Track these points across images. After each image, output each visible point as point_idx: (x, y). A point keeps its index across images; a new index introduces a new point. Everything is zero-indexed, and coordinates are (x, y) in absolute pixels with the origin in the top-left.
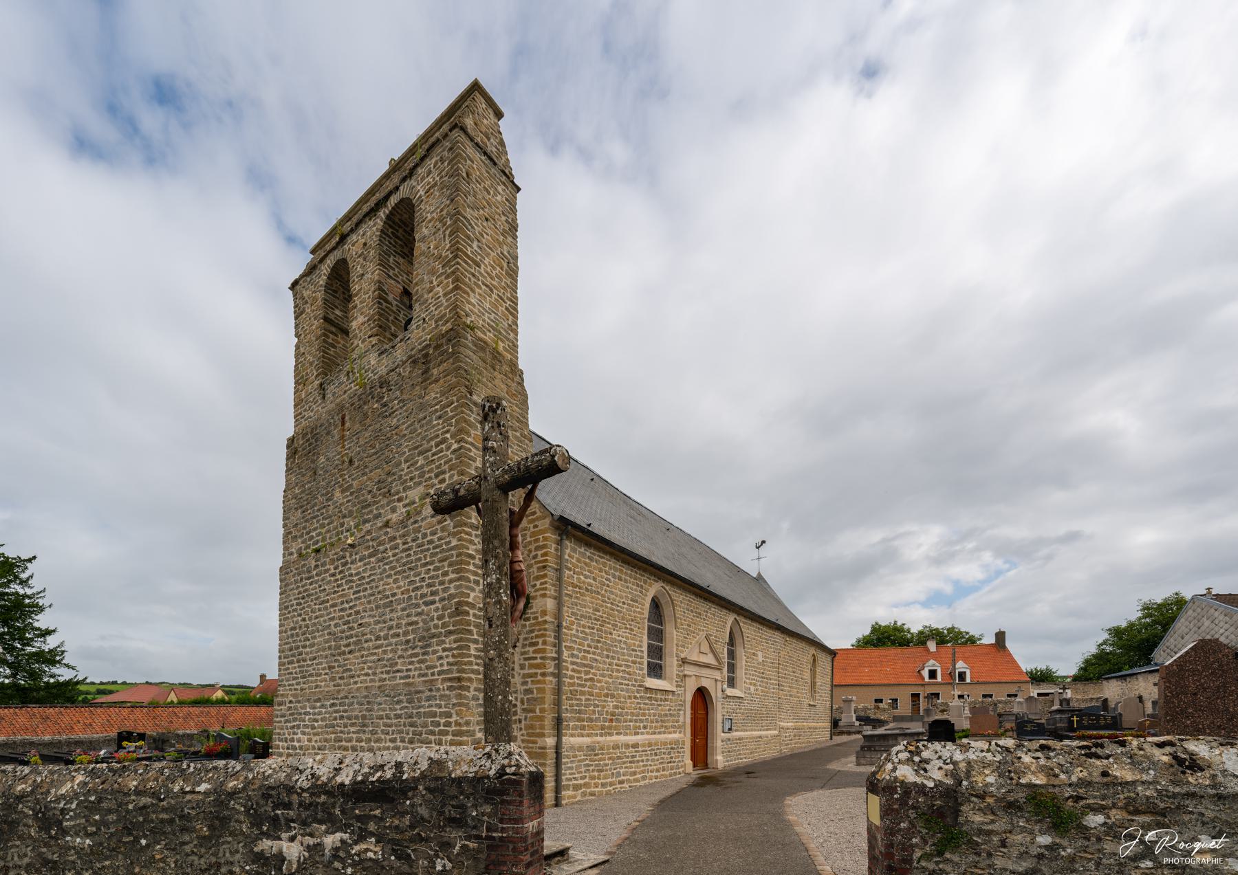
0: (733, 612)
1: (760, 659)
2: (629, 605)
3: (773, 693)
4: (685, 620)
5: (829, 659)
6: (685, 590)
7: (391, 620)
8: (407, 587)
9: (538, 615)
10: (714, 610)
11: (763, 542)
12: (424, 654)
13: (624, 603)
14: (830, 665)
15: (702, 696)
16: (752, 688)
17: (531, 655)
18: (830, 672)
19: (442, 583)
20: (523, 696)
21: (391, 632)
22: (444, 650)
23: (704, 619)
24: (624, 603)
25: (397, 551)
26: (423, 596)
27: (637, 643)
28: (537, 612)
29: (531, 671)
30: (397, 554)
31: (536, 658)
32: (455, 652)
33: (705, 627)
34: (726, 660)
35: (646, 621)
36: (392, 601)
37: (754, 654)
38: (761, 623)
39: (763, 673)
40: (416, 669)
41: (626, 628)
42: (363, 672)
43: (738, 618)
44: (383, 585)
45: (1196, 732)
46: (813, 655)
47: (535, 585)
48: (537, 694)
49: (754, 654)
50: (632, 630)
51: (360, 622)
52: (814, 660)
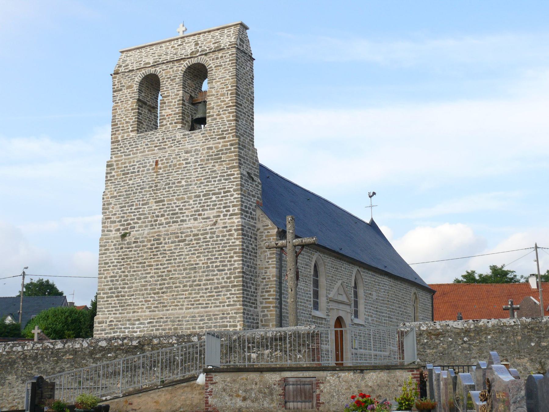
0: (357, 265)
1: (374, 297)
2: (305, 268)
3: (385, 323)
4: (330, 274)
5: (429, 296)
6: (330, 255)
7: (194, 277)
8: (206, 261)
9: (271, 277)
10: (346, 265)
11: (374, 193)
12: (217, 296)
13: (303, 267)
14: (430, 301)
15: (339, 322)
16: (370, 318)
17: (267, 297)
18: (431, 307)
19: (229, 261)
20: (262, 318)
21: (195, 283)
22: (231, 294)
23: (340, 272)
24: (303, 267)
25: (199, 241)
26: (216, 266)
27: (308, 289)
28: (270, 275)
29: (266, 305)
30: (199, 243)
31: (269, 299)
32: (238, 295)
33: (340, 277)
34: (353, 299)
35: (312, 276)
36: (195, 267)
37: (370, 294)
38: (374, 272)
39: (377, 308)
40: (212, 303)
41: (304, 281)
42: (174, 304)
43: (359, 269)
44: (189, 258)
45: (450, 319)
46: (415, 293)
47: (268, 262)
48: (270, 317)
49: (370, 294)
50: (306, 282)
51: (171, 277)
52: (416, 298)
